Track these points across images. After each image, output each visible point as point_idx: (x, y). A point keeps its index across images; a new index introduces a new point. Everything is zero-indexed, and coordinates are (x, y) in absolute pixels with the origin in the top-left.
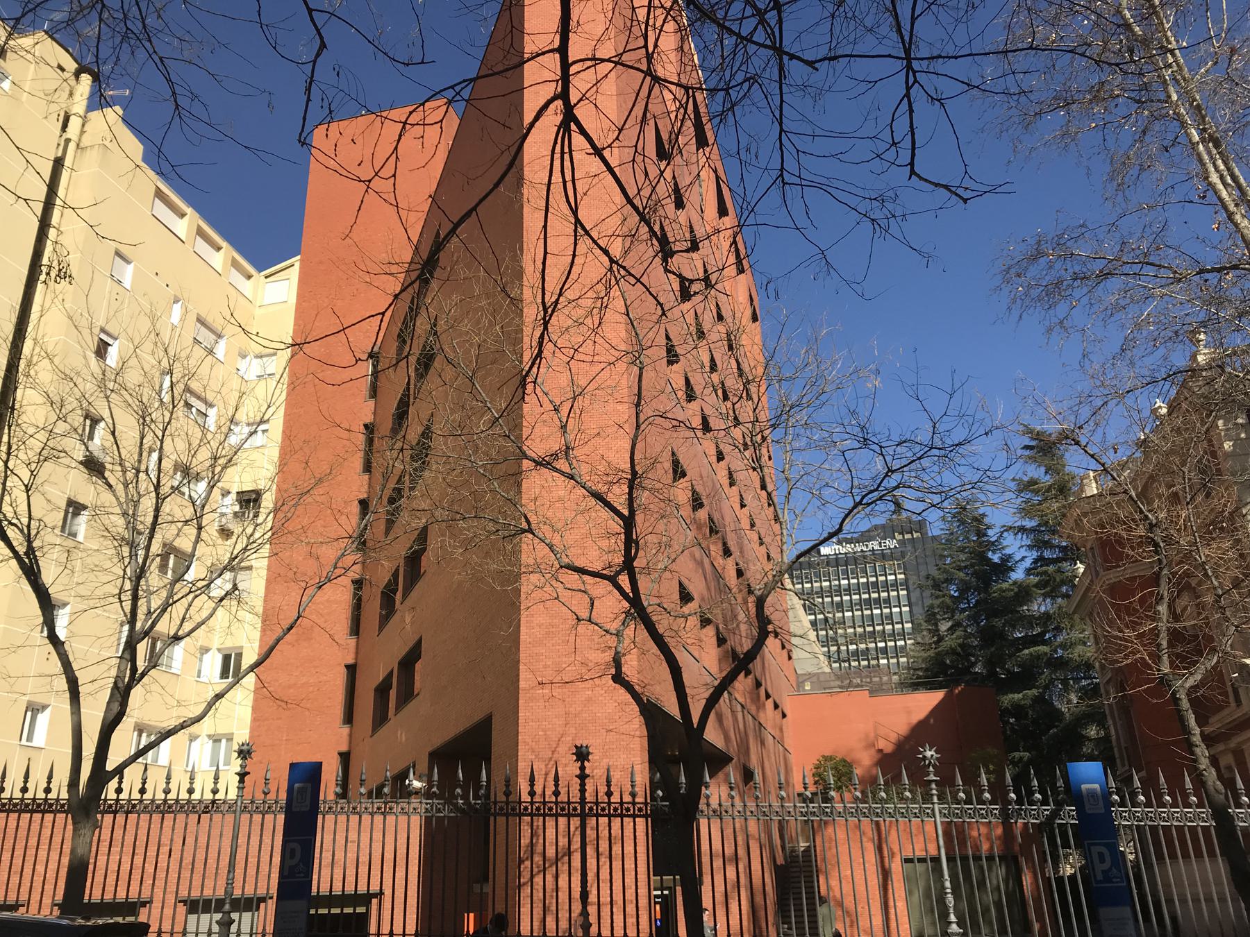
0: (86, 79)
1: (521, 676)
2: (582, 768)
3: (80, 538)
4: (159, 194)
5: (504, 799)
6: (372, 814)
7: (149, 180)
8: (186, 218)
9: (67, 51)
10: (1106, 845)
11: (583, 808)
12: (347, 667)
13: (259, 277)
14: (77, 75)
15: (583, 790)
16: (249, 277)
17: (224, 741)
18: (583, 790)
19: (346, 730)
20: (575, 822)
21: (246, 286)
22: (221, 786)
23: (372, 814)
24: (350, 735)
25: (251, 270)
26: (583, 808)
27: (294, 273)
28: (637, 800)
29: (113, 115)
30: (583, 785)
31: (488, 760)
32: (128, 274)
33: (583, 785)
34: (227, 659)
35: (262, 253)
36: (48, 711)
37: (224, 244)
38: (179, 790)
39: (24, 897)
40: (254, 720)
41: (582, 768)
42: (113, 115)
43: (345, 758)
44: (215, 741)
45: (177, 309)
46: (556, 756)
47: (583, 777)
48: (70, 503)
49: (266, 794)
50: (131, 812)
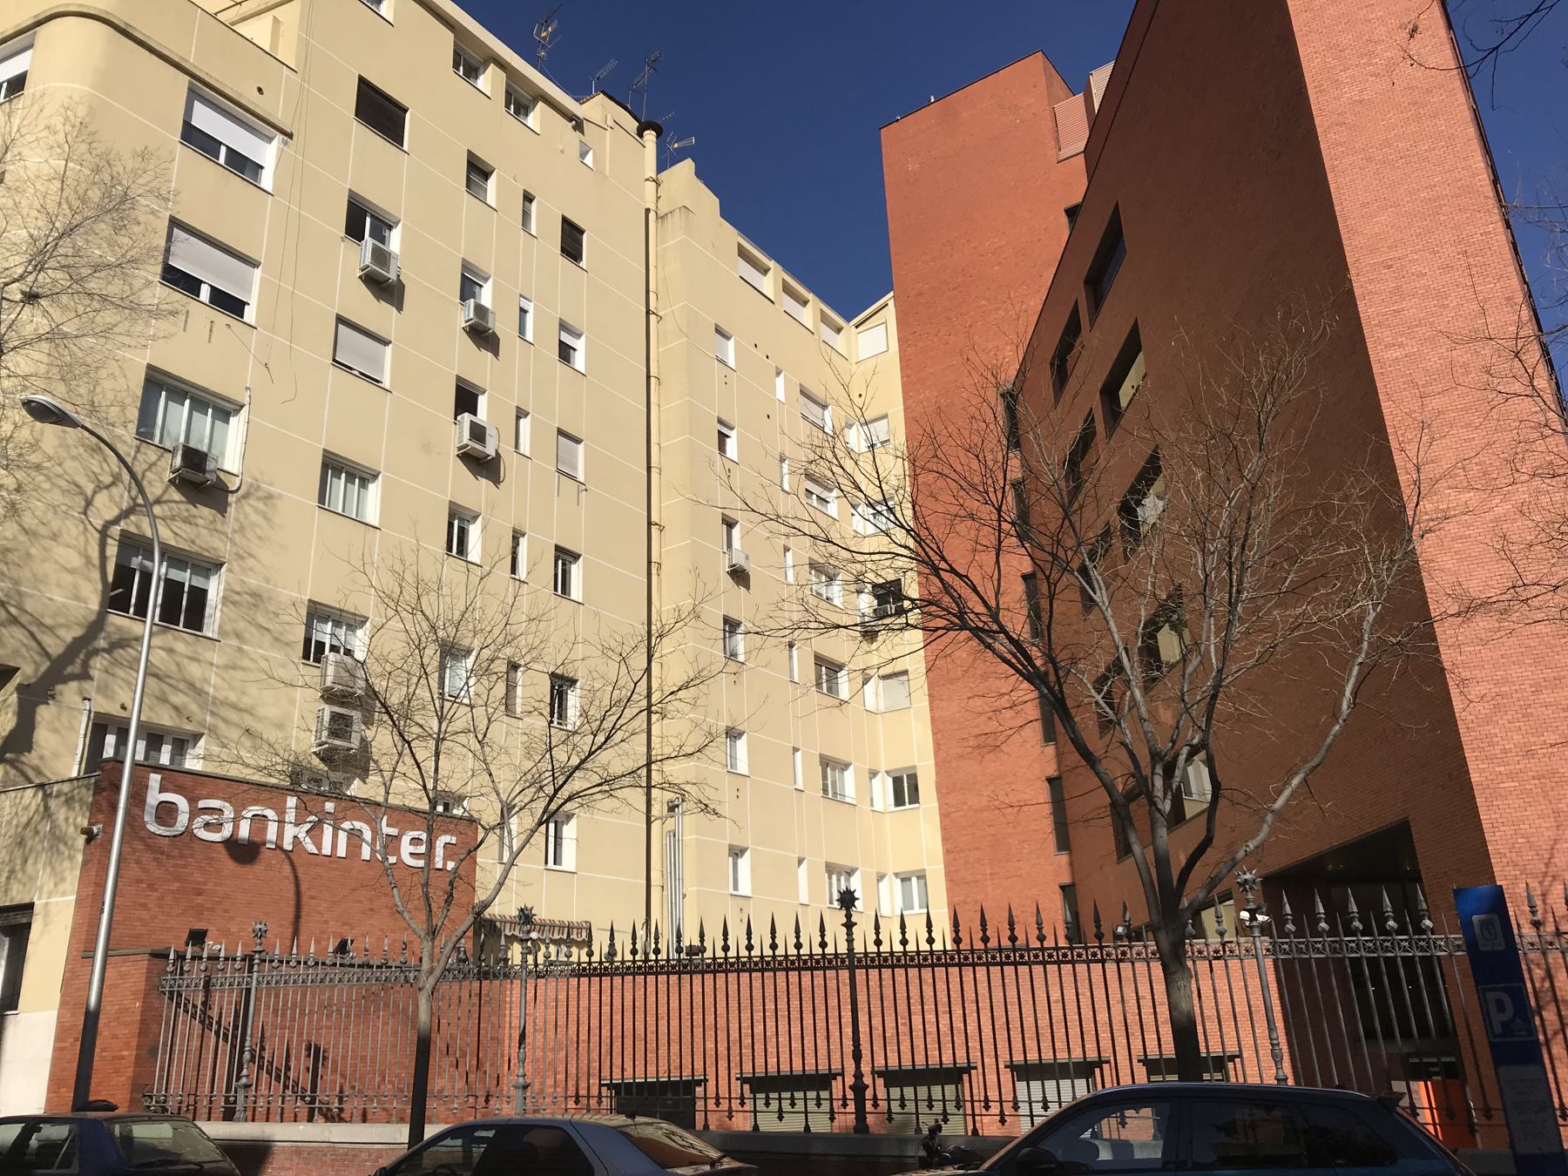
0: (650, 136)
1: (1471, 766)
2: (848, 916)
3: (741, 658)
4: (742, 253)
5: (982, 946)
6: (1118, 961)
7: (732, 237)
8: (770, 273)
9: (626, 109)
10: (1505, 990)
11: (851, 961)
12: (1050, 780)
13: (849, 328)
14: (640, 135)
15: (850, 941)
16: (839, 330)
17: (914, 879)
18: (850, 941)
19: (1063, 858)
20: (845, 974)
21: (838, 341)
22: (829, 939)
23: (1103, 961)
24: (1071, 864)
25: (840, 321)
26: (851, 961)
27: (890, 314)
28: (1046, 945)
29: (687, 167)
30: (850, 934)
31: (1419, 880)
32: (730, 350)
33: (850, 934)
34: (897, 782)
35: (848, 300)
36: (747, 854)
37: (810, 296)
38: (891, 941)
39: (836, 1066)
40: (947, 852)
41: (848, 916)
42: (687, 167)
43: (1068, 891)
44: (903, 880)
45: (780, 381)
46: (1552, 869)
47: (849, 925)
48: (727, 620)
49: (1222, 934)
50: (1122, 961)
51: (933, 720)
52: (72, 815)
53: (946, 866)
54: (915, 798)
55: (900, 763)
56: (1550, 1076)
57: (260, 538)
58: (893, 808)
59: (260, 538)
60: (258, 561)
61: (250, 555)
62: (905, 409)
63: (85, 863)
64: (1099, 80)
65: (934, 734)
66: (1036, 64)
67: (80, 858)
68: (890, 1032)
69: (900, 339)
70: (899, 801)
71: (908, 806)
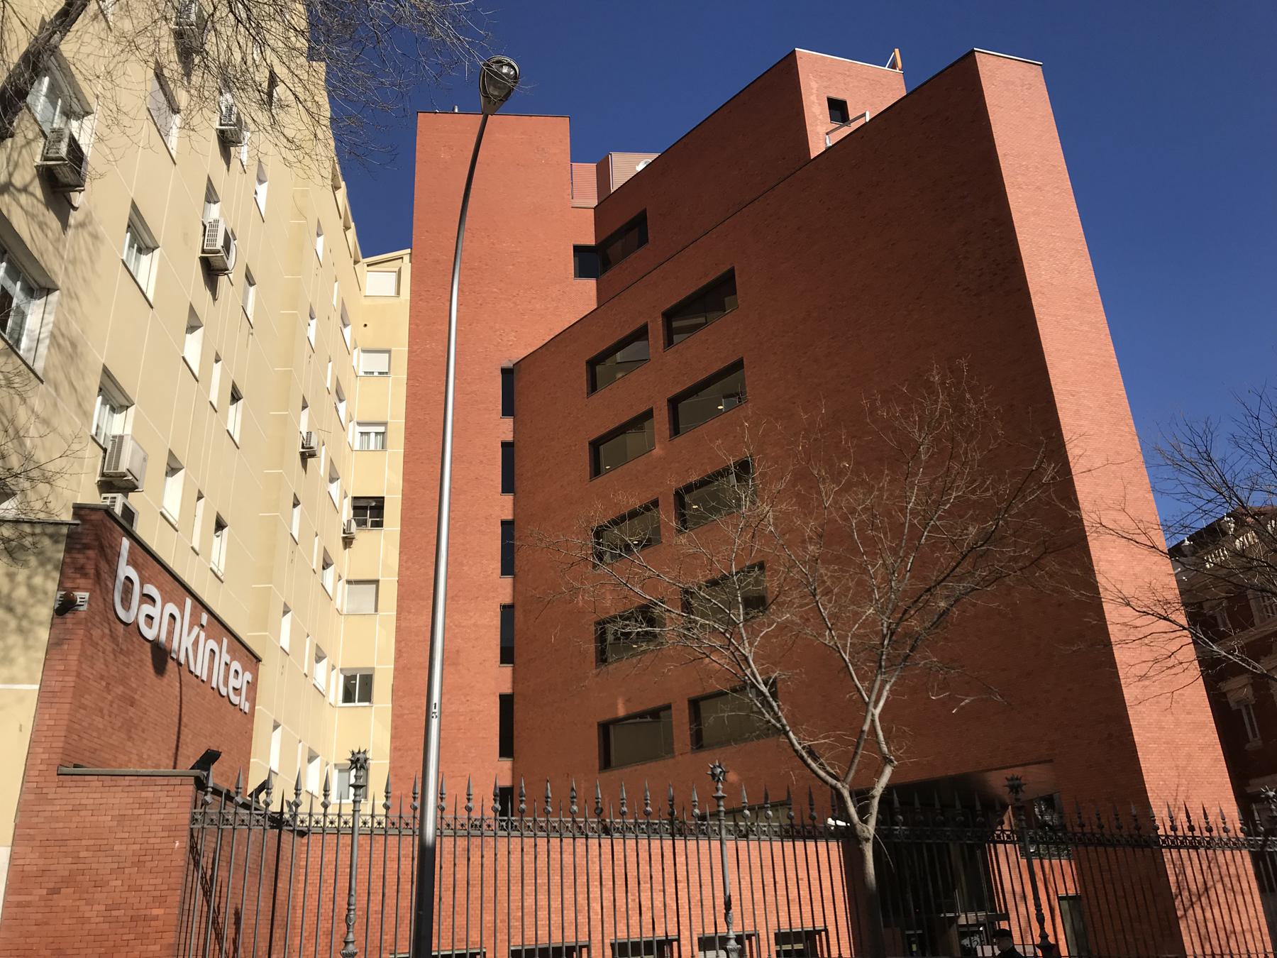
44: (340, 771)
51: (398, 628)
52: (22, 574)
53: (392, 761)
54: (367, 696)
55: (358, 662)
56: (985, 886)
57: (84, 280)
58: (340, 704)
59: (84, 280)
60: (81, 306)
61: (78, 298)
62: (410, 352)
63: (54, 645)
64: (628, 165)
65: (397, 641)
66: (561, 126)
67: (44, 634)
68: (516, 888)
69: (412, 292)
70: (348, 697)
71: (357, 704)
